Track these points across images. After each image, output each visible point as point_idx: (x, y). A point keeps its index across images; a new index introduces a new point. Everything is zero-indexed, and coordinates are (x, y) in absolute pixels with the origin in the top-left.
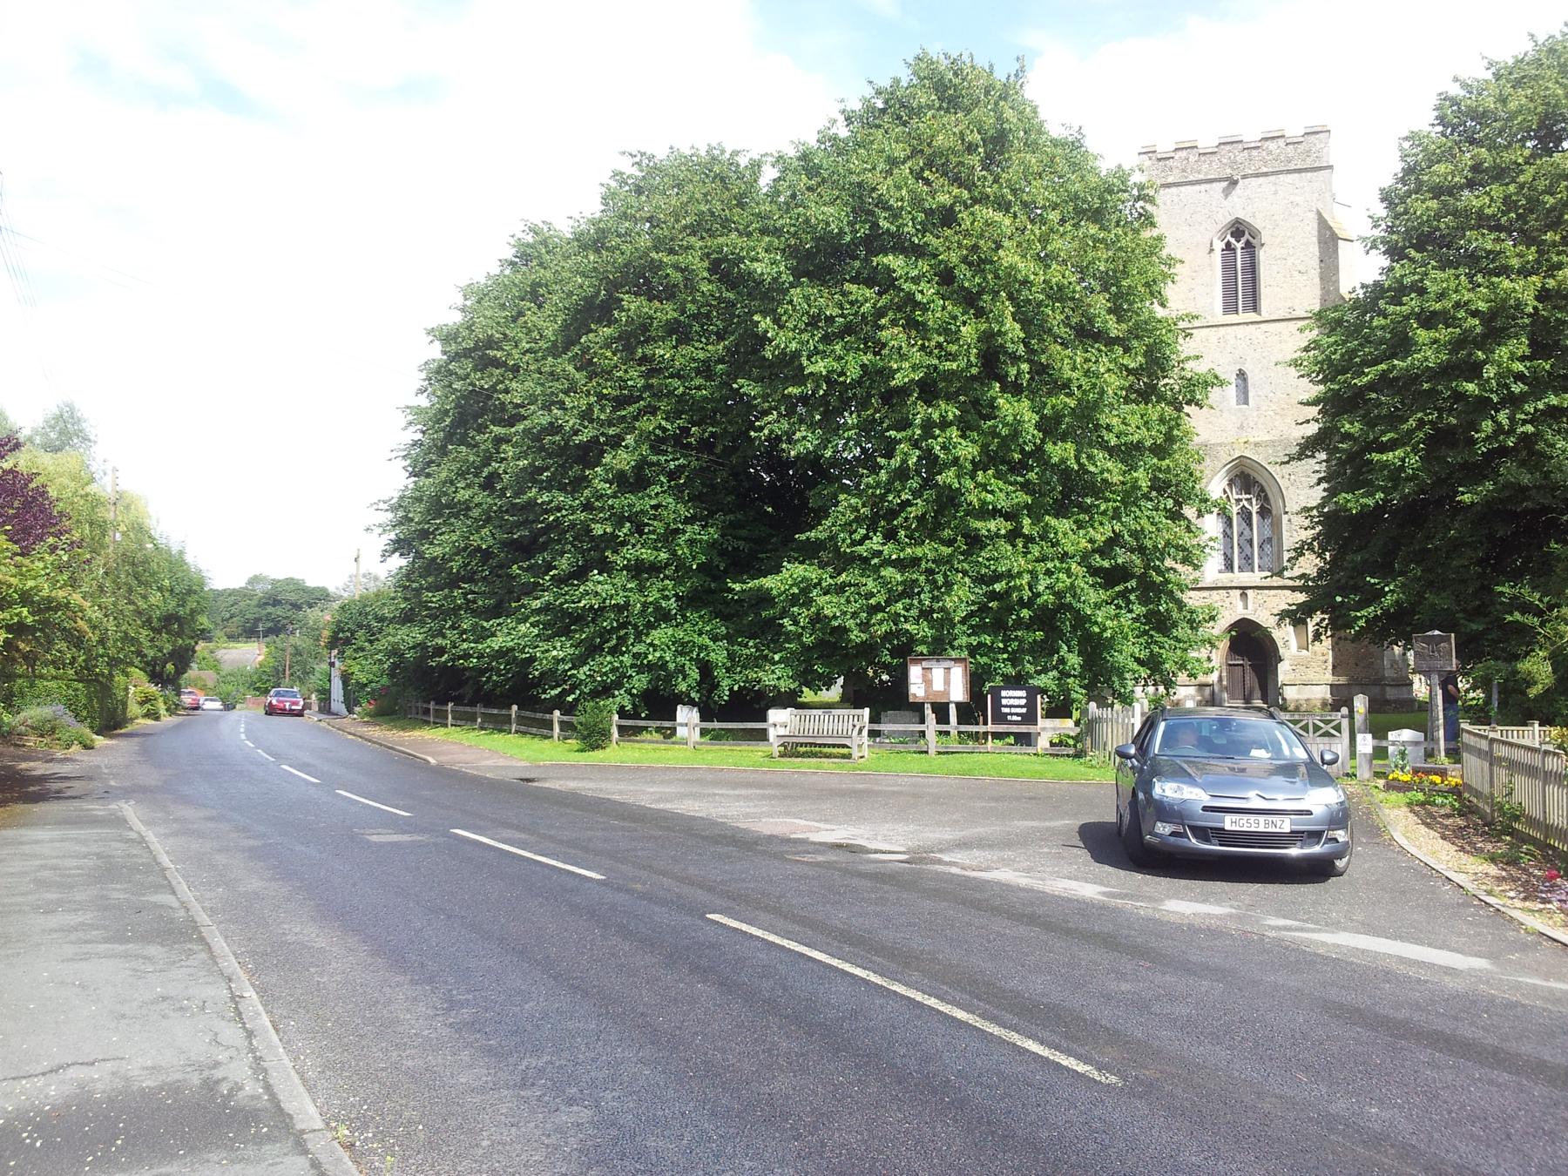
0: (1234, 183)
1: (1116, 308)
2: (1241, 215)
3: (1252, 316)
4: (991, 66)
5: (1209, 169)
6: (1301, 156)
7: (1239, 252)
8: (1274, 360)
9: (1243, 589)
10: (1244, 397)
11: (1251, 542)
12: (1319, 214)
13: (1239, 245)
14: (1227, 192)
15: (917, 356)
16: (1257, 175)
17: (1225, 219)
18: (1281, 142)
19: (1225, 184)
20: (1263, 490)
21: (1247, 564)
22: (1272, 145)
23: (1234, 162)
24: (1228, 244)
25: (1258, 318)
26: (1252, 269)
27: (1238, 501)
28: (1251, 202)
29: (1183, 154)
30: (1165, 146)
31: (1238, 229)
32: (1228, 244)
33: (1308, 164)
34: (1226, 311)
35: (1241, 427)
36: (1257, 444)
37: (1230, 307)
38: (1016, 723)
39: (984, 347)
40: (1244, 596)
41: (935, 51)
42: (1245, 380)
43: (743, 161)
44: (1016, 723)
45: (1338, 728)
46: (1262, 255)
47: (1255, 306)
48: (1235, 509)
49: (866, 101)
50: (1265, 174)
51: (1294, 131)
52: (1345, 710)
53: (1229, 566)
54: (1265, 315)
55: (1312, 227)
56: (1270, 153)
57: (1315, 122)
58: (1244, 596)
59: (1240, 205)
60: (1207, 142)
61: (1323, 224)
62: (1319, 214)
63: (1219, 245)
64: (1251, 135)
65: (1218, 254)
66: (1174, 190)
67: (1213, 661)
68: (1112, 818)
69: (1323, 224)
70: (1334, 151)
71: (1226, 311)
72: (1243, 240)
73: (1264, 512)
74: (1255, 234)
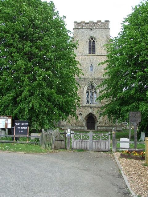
0: (92, 29)
1: (64, 52)
2: (93, 35)
4: (52, 2)
5: (87, 26)
6: (104, 25)
7: (92, 42)
12: (107, 37)
18: (100, 23)
22: (99, 23)
23: (92, 26)
24: (90, 41)
26: (94, 46)
28: (95, 33)
29: (82, 23)
30: (79, 21)
31: (92, 38)
32: (90, 41)
34: (89, 54)
35: (91, 75)
36: (94, 79)
37: (90, 53)
38: (21, 133)
44: (21, 133)
46: (96, 43)
49: (56, 14)
51: (103, 21)
54: (96, 54)
56: (98, 24)
57: (107, 20)
59: (92, 33)
60: (87, 21)
62: (107, 37)
64: (95, 21)
67: (36, 93)
68: (10, 119)
70: (111, 26)
71: (89, 54)
72: (93, 40)
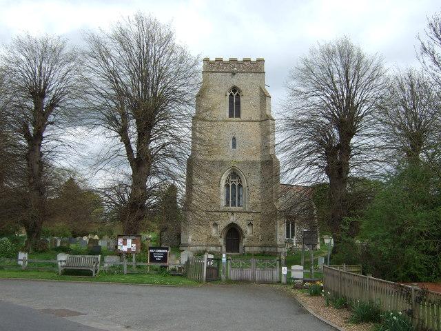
8: (236, 136)
10: (234, 146)
11: (235, 196)
13: (235, 95)
15: (247, 249)
16: (242, 72)
21: (234, 204)
22: (246, 63)
24: (231, 94)
25: (240, 120)
26: (238, 103)
28: (242, 81)
30: (212, 59)
31: (235, 89)
32: (231, 94)
36: (238, 162)
37: (231, 115)
39: (118, 229)
41: (146, 15)
46: (242, 99)
47: (238, 115)
53: (228, 204)
55: (258, 91)
59: (234, 81)
63: (228, 94)
65: (228, 97)
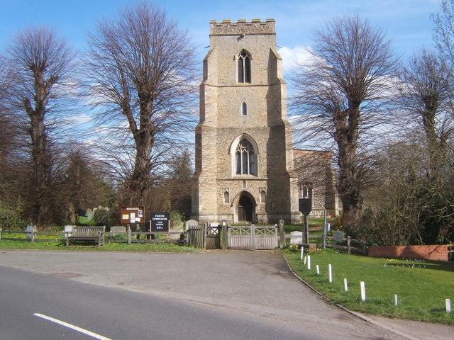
0: (242, 36)
3: (248, 84)
5: (234, 31)
9: (244, 180)
12: (271, 50)
14: (239, 39)
16: (250, 35)
17: (240, 50)
18: (259, 24)
19: (237, 37)
20: (251, 145)
21: (245, 172)
22: (255, 24)
25: (255, 178)
27: (243, 149)
28: (249, 43)
31: (244, 53)
33: (268, 32)
37: (241, 80)
38: (159, 221)
40: (244, 182)
42: (248, 61)
43: (126, 23)
45: (274, 231)
47: (249, 80)
48: (242, 152)
50: (253, 34)
52: (276, 225)
54: (252, 83)
58: (244, 182)
61: (271, 53)
62: (271, 50)
63: (237, 58)
65: (237, 61)
66: (222, 37)
69: (271, 53)
73: (251, 153)
74: (249, 55)
